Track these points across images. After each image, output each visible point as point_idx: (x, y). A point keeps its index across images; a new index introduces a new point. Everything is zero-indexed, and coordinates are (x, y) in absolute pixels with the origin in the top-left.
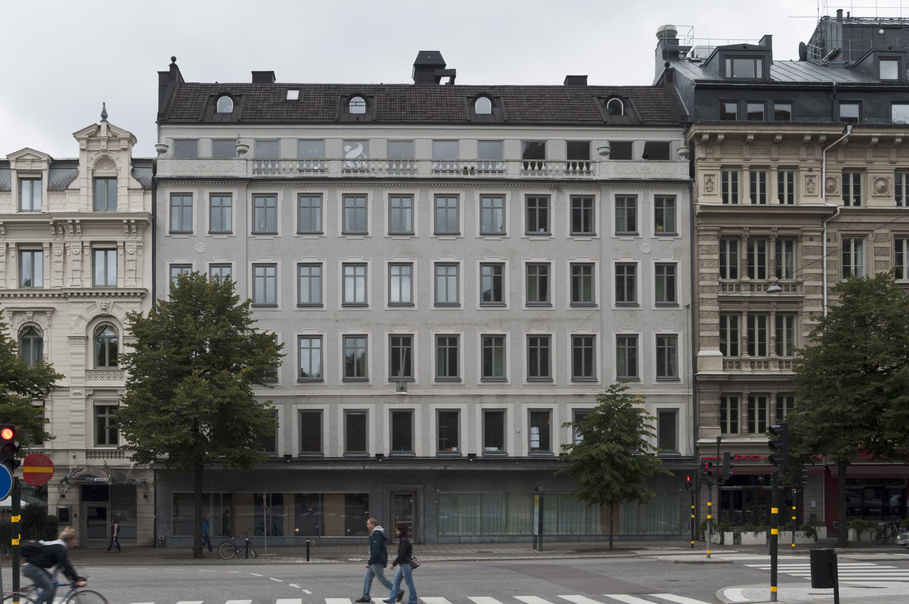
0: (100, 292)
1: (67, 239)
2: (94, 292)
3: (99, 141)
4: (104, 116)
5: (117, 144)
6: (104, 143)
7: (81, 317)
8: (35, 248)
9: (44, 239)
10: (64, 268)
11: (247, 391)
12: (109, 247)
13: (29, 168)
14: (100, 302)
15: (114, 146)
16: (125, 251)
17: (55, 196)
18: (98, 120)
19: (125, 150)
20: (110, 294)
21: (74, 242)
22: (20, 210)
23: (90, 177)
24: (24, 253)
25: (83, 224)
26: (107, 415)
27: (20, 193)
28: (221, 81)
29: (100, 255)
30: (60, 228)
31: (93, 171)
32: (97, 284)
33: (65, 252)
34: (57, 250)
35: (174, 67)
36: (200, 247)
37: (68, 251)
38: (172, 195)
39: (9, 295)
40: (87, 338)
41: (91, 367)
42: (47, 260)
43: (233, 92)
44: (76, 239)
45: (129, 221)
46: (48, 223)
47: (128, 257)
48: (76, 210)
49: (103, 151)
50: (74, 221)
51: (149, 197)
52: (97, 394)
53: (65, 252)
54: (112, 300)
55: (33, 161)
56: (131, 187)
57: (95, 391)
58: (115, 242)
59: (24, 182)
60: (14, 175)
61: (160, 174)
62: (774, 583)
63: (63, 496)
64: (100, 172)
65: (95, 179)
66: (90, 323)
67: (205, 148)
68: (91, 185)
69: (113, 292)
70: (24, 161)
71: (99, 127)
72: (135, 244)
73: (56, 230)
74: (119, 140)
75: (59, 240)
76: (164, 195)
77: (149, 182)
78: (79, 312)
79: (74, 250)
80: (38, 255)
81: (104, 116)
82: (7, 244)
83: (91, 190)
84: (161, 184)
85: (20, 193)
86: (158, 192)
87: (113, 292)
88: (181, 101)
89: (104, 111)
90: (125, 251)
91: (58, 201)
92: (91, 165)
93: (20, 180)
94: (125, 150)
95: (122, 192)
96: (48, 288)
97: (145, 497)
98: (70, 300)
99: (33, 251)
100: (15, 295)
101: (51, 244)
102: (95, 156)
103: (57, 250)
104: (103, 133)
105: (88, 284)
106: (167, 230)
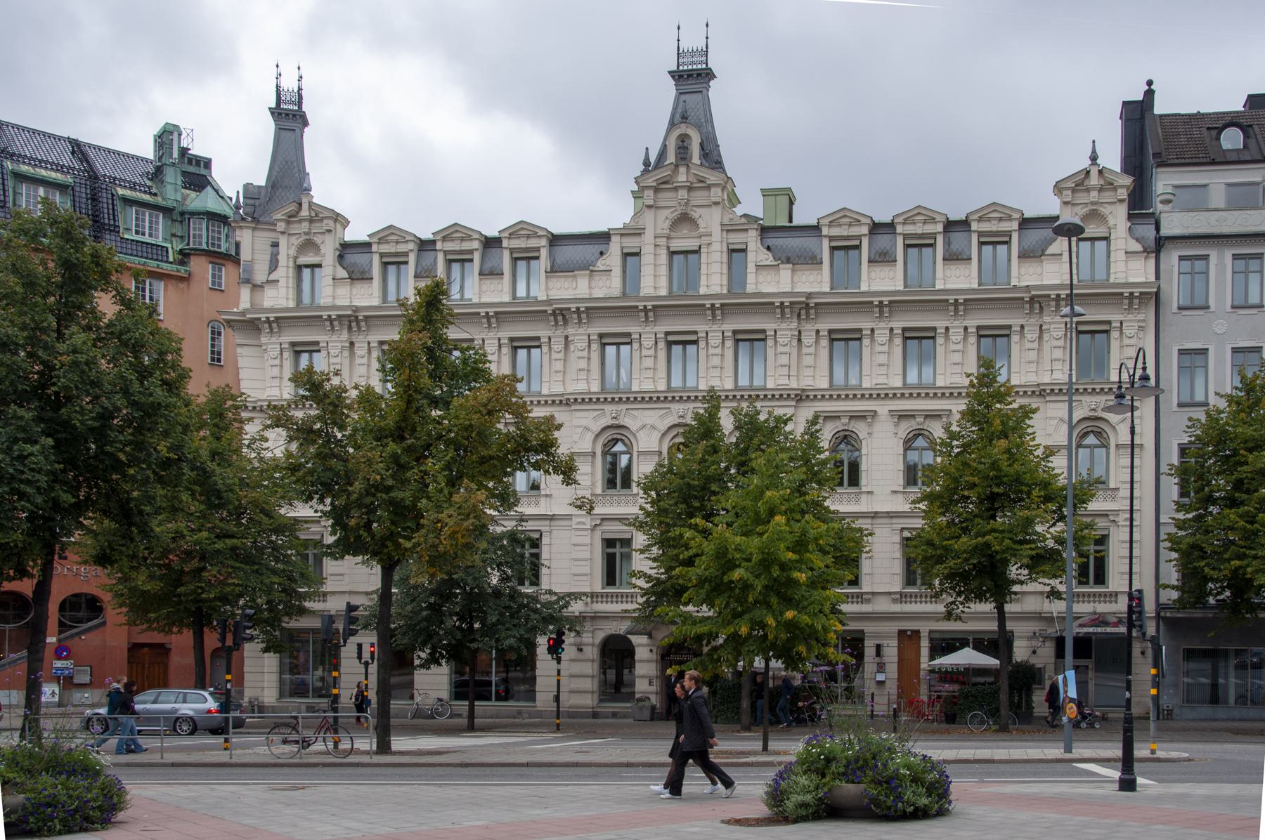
0: (677, 395)
1: (1046, 319)
2: (670, 395)
3: (300, 221)
4: (1094, 158)
5: (1112, 193)
6: (1094, 194)
7: (587, 429)
8: (532, 343)
9: (542, 332)
10: (589, 364)
11: (823, 515)
12: (623, 339)
13: (994, 229)
14: (609, 408)
15: (316, 228)
16: (776, 342)
17: (1027, 265)
18: (1086, 163)
19: (329, 231)
20: (1085, 390)
21: (580, 335)
22: (514, 297)
23: (291, 264)
24: (608, 348)
25: (279, 322)
26: (618, 550)
27: (514, 276)
28: (1182, 112)
29: (611, 350)
30: (1037, 306)
31: (295, 258)
32: (835, 382)
33: (1040, 337)
34: (1032, 334)
35: (1150, 93)
36: (1220, 327)
37: (1046, 336)
38: (1181, 258)
39: (951, 394)
40: (594, 454)
41: (599, 491)
42: (546, 358)
43: (1244, 122)
44: (581, 331)
45: (330, 316)
46: (546, 311)
47: (1127, 341)
48: (893, 288)
49: (1092, 203)
50: (713, 305)
51: (1152, 262)
52: (605, 523)
53: (1040, 337)
54: (623, 407)
55: (1000, 219)
56: (1129, 250)
57: (602, 520)
58: (696, 333)
59: (519, 263)
60: (506, 254)
61: (1164, 232)
62: (336, 732)
63: (1034, 652)
64: (303, 260)
65: (299, 268)
66: (597, 436)
67: (1217, 196)
68: (725, 259)
69: (624, 396)
70: (989, 220)
71: (1088, 172)
72: (339, 344)
73: (1032, 308)
74: (322, 220)
75: (559, 332)
76: (1171, 258)
77: (1152, 243)
78: (584, 423)
79: (1055, 334)
80: (625, 349)
81: (1094, 158)
82: (966, 328)
83: (725, 266)
84: (1168, 245)
85: (514, 276)
86: (1162, 255)
87: (624, 396)
88: (1152, 139)
89: (1094, 151)
90: (776, 342)
91: (1031, 270)
92: (292, 252)
93: (515, 260)
94: (329, 231)
95: (1118, 256)
96: (942, 385)
97: (1143, 653)
98: (574, 407)
99: (311, 352)
100: (943, 394)
101: (947, 329)
102: (296, 241)
103: (558, 345)
104: (1094, 180)
105: (662, 386)
106: (1175, 305)
